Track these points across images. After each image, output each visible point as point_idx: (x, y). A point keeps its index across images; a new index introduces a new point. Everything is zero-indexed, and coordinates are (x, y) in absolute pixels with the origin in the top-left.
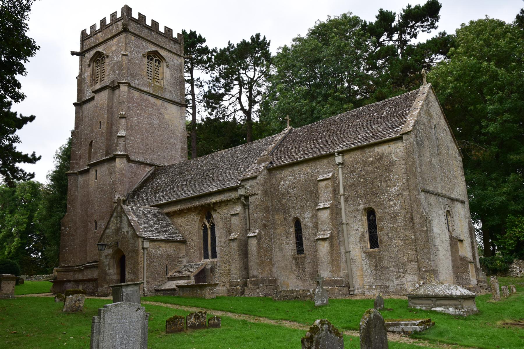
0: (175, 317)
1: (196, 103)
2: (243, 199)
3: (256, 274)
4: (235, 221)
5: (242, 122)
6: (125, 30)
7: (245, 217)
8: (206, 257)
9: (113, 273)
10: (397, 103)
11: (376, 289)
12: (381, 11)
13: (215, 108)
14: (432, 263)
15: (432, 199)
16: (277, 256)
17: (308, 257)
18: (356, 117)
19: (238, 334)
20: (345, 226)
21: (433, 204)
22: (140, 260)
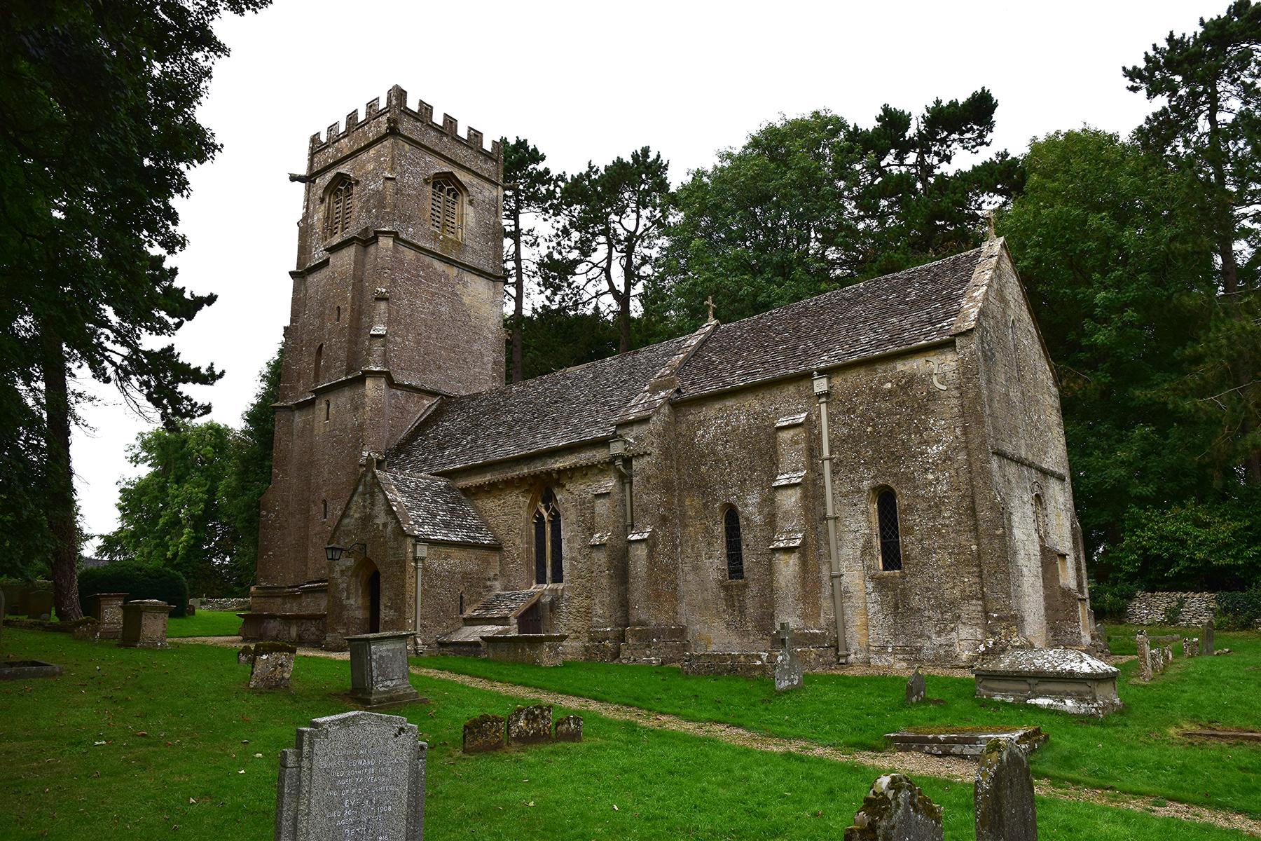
0: (485, 719)
1: (524, 277)
2: (619, 462)
3: (643, 617)
4: (602, 507)
5: (610, 317)
6: (393, 132)
7: (623, 501)
8: (541, 579)
9: (355, 605)
10: (936, 274)
11: (894, 653)
12: (886, 109)
13: (559, 288)
14: (1013, 603)
15: (1012, 469)
16: (688, 582)
17: (752, 584)
18: (853, 302)
19: (624, 762)
20: (831, 523)
21: (1013, 481)
22: (410, 581)
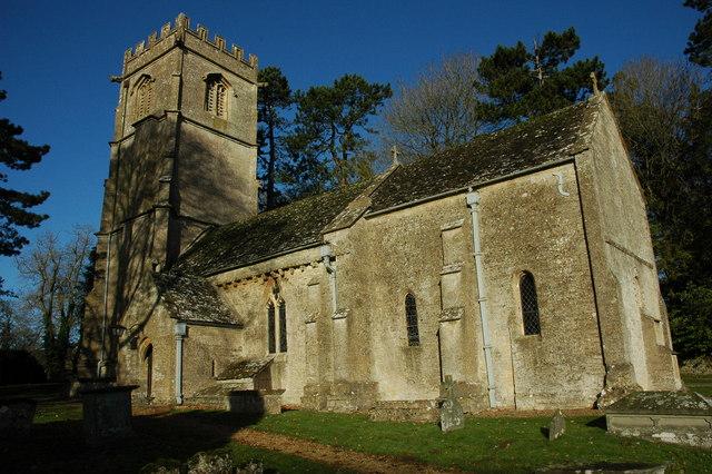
15: (620, 255)
